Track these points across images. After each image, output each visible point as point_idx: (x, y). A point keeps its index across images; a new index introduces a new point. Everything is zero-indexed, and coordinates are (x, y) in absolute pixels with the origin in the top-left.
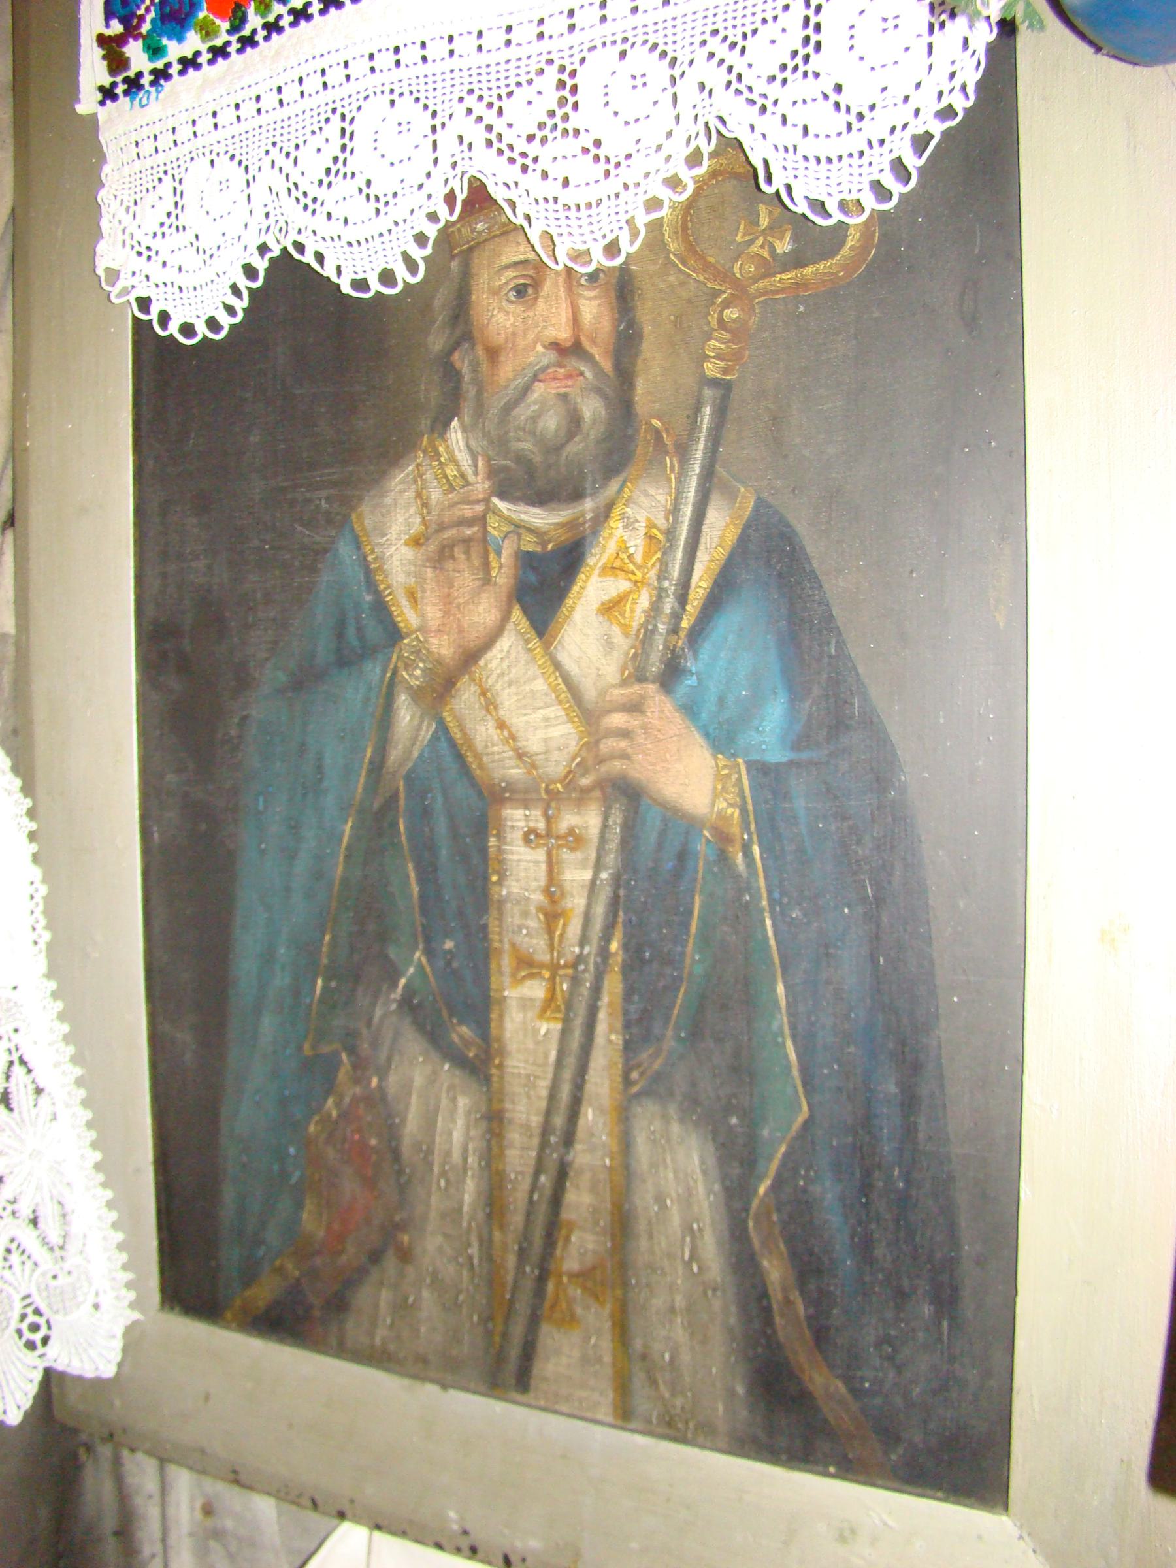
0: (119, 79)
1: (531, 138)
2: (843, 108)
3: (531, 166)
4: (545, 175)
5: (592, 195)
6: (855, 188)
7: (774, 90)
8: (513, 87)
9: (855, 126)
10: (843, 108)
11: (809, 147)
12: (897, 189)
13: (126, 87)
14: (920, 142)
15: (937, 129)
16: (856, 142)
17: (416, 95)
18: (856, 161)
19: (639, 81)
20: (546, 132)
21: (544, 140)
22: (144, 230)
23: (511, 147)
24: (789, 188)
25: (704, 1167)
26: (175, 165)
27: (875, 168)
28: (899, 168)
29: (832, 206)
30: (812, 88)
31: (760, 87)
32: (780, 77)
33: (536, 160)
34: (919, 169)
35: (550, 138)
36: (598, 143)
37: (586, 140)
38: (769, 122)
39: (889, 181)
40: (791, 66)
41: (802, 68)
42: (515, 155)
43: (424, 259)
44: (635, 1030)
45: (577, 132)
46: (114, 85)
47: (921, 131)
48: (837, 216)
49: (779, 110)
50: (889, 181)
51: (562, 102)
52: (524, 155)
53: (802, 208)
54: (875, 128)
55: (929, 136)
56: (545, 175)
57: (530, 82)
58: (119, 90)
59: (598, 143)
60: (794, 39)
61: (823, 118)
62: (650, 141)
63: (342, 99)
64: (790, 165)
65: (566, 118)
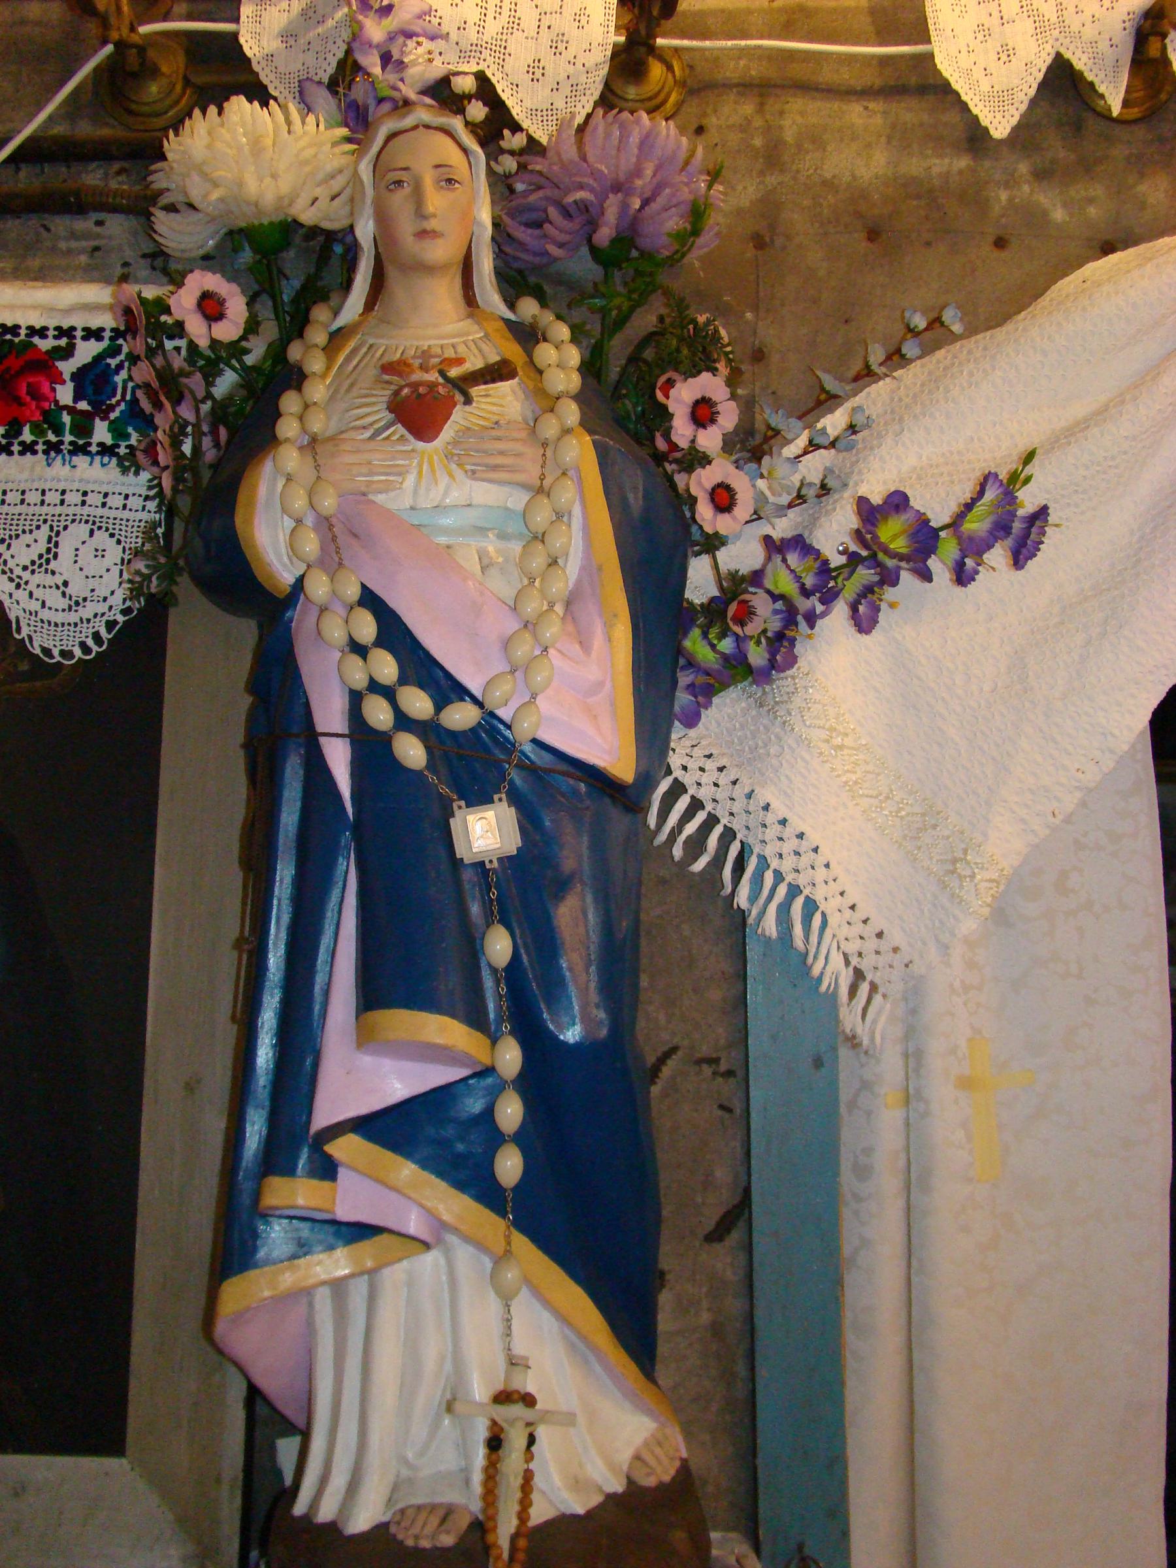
0: (41, 441)
1: (25, 568)
2: (68, 596)
3: (23, 586)
4: (31, 595)
5: (60, 618)
6: (71, 643)
7: (26, 575)
8: (20, 532)
9: (74, 608)
10: (68, 596)
11: (45, 614)
12: (95, 648)
13: (36, 448)
14: (110, 625)
15: (121, 619)
16: (73, 617)
17: (111, 531)
18: (72, 628)
19: (100, 553)
20: (35, 567)
21: (33, 572)
22: (16, 560)
23: (11, 571)
24: (30, 637)
25: (516, 1396)
26: (56, 518)
27: (83, 635)
28: (97, 637)
29: (56, 652)
30: (49, 580)
31: (18, 571)
32: (31, 568)
33: (27, 583)
34: (109, 640)
35: (37, 570)
36: (66, 584)
37: (59, 580)
38: (21, 595)
39: (90, 642)
40: (38, 562)
41: (45, 566)
42: (14, 576)
43: (109, 640)
44: (1149, 22)
45: (53, 573)
46: (35, 443)
47: (111, 618)
48: (58, 658)
49: (29, 587)
50: (90, 642)
51: (49, 550)
52: (20, 577)
53: (38, 651)
54: (87, 611)
55: (115, 622)
56: (31, 595)
57: (31, 531)
58: (40, 447)
59: (66, 584)
60: (42, 547)
61: (55, 599)
62: (103, 592)
63: (134, 521)
64: (32, 623)
65: (48, 561)
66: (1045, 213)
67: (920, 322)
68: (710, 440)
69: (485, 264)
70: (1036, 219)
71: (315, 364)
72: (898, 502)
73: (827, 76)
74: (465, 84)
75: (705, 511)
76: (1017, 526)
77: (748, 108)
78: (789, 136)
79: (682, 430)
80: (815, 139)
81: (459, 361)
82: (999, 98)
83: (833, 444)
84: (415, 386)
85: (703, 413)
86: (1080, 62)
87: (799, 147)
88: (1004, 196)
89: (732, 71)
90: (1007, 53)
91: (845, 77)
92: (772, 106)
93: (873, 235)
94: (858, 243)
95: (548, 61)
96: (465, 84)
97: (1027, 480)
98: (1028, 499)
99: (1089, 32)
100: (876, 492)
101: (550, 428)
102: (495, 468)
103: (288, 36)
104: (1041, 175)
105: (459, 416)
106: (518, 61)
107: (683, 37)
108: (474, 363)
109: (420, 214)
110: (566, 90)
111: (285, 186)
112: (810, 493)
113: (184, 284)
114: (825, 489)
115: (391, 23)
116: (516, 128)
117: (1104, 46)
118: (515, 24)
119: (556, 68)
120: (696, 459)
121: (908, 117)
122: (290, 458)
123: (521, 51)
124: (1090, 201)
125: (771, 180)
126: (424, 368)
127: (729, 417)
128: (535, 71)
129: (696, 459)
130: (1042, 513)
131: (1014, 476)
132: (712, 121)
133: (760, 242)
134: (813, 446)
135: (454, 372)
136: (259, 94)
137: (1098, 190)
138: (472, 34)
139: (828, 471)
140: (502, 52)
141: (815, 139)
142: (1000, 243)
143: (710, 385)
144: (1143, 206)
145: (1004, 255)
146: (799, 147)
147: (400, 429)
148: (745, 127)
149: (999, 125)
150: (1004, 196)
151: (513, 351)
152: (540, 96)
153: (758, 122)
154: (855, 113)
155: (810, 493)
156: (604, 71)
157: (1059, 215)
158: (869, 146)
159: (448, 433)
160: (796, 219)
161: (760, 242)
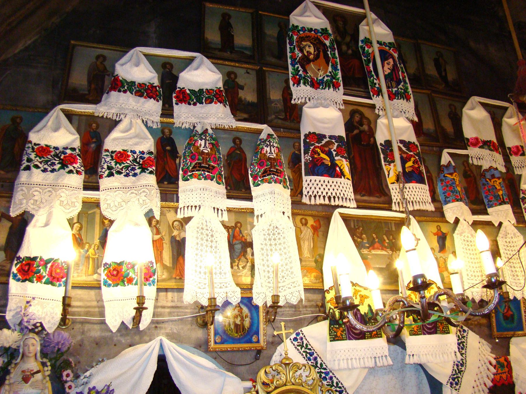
66: (121, 341)
67: (101, 360)
68: (69, 379)
69: (39, 355)
70: (119, 341)
71: (12, 371)
72: (94, 388)
73: (92, 321)
74: (38, 325)
75: (67, 390)
76: (109, 392)
77: (80, 326)
78: (86, 330)
79: (65, 378)
80: (89, 330)
81: (32, 370)
82: (115, 326)
83: (87, 377)
84: (26, 375)
85: (68, 375)
86: (125, 322)
87: (87, 331)
88: (116, 338)
89: (78, 320)
90: (116, 320)
91: (94, 321)
92: (84, 325)
93: (97, 344)
94: (94, 345)
95: (51, 320)
96: (38, 325)
97: (227, 208)
98: (111, 389)
99: (127, 319)
100: (91, 387)
101: (44, 381)
102: (36, 387)
103: (13, 316)
104: (121, 336)
105: (32, 380)
106: (47, 320)
107: (278, 14)
108: (35, 370)
109: (29, 350)
110: (53, 324)
111: (10, 344)
112: (85, 383)
113: (143, 151)
114: (87, 383)
115: (28, 317)
116: (45, 330)
117: (128, 320)
118: (47, 315)
119: (52, 321)
120: (66, 382)
121: (103, 327)
122: (7, 387)
123: (47, 319)
124: (128, 339)
125: (83, 336)
126: (28, 372)
127: (72, 375)
128: (49, 322)
129: (66, 382)
130: (113, 390)
131: (109, 385)
132: (75, 327)
133: (80, 345)
134: (84, 378)
135: (32, 372)
136: (9, 328)
137: (129, 338)
138: (40, 316)
139: (87, 380)
140: (44, 318)
141: (89, 330)
142: (115, 345)
143: (69, 371)
144: (135, 340)
145: (116, 347)
146: (87, 331)
147: (23, 382)
148: (79, 328)
149: (114, 330)
150: (116, 338)
151: (41, 367)
152: (50, 325)
153: (82, 327)
154: (96, 327)
155: (85, 383)
156: (59, 321)
157: (123, 341)
158: (97, 331)
159: (30, 382)
160: (86, 343)
161: (80, 345)
